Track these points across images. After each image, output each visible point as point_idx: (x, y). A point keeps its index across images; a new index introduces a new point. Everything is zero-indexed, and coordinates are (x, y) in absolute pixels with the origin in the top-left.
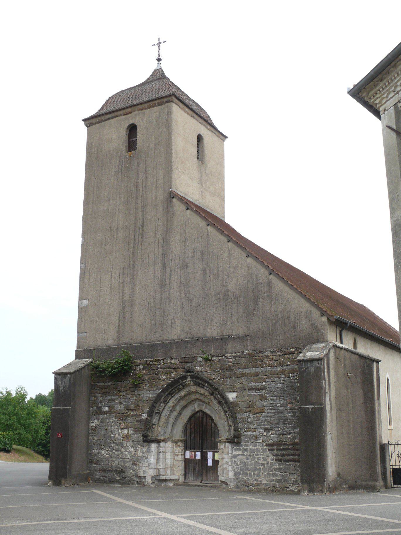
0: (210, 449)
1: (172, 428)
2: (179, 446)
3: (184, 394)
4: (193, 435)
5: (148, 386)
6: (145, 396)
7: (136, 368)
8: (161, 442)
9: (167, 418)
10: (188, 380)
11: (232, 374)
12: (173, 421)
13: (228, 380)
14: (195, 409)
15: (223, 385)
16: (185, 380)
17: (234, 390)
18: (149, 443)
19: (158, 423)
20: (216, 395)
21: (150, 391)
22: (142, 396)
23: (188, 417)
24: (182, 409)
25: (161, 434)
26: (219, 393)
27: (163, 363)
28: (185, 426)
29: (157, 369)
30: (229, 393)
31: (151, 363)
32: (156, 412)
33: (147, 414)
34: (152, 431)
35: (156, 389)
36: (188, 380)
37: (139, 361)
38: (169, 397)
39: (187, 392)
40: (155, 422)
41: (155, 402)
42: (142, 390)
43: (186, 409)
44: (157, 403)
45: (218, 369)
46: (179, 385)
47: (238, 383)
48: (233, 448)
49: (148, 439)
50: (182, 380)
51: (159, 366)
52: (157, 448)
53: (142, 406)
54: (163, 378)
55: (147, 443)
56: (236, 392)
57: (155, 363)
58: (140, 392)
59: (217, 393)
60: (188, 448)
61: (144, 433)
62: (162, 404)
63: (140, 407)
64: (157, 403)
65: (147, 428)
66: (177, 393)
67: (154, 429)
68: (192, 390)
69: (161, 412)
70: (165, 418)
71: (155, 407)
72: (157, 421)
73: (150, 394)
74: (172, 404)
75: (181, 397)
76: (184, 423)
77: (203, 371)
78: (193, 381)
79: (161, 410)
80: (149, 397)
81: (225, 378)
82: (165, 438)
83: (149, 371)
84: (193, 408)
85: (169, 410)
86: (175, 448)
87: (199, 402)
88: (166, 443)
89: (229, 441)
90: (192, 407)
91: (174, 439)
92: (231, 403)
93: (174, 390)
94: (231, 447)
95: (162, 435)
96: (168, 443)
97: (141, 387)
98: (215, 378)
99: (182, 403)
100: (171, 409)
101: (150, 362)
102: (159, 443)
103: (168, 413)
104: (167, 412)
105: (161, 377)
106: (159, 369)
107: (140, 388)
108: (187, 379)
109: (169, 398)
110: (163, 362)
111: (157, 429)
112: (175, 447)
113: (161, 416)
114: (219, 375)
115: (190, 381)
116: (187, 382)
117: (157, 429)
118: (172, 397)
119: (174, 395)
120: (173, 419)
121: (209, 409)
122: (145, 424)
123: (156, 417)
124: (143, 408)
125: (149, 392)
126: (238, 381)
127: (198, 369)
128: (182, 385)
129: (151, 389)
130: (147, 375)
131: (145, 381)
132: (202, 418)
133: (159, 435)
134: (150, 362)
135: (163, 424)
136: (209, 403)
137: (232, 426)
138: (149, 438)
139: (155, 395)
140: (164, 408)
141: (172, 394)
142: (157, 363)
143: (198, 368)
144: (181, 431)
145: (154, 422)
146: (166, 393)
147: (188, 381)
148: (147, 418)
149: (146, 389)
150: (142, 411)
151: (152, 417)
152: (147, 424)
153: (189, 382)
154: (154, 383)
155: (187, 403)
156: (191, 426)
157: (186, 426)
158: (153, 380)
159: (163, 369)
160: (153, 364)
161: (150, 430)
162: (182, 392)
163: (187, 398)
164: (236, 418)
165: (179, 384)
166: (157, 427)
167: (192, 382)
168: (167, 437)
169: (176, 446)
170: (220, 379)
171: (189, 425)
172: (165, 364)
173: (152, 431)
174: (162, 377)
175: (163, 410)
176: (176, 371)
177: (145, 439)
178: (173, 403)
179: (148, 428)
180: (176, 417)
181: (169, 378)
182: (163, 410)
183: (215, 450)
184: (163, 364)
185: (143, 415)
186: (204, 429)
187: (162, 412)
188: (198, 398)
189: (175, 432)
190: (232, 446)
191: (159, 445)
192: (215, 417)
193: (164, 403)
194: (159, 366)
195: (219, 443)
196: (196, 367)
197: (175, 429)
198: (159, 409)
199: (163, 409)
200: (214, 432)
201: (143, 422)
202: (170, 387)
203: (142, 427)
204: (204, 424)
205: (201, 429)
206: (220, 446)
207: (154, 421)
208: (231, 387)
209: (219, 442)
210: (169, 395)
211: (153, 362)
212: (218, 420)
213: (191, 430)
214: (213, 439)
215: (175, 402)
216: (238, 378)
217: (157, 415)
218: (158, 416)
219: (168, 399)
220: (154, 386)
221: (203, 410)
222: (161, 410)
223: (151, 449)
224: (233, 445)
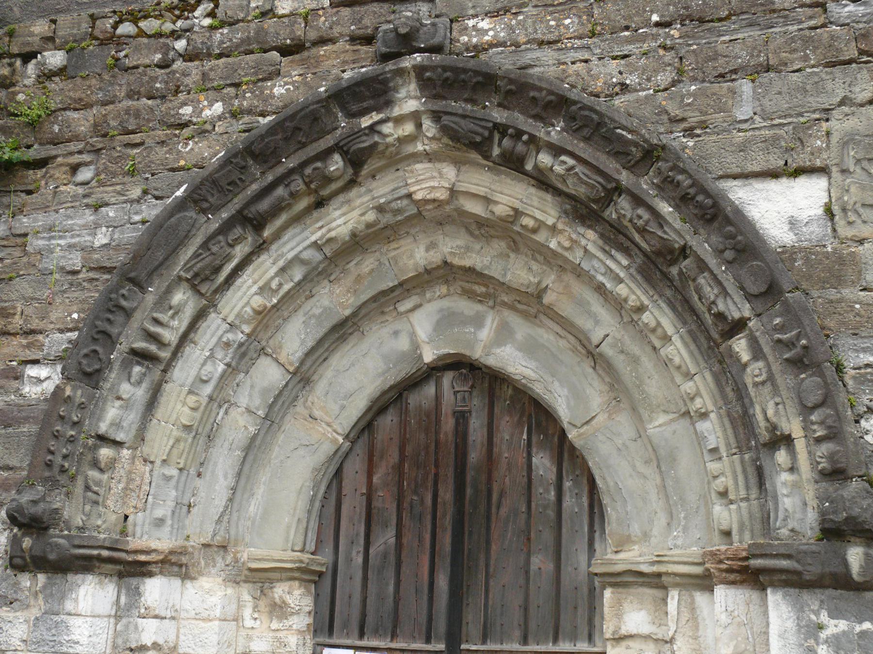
0: (517, 633)
1: (239, 474)
2: (279, 610)
3: (350, 226)
4: (385, 539)
5: (85, 174)
6: (62, 242)
7: (14, 72)
8: (151, 575)
9: (211, 399)
10: (396, 111)
11: (780, 41)
12: (252, 429)
13: (745, 87)
14: (416, 346)
15: (703, 125)
16: (378, 110)
17: (802, 159)
18: (58, 578)
19: (141, 437)
20: (638, 201)
21: (97, 208)
22: (41, 243)
23: (358, 406)
24: (320, 342)
25: (159, 513)
26: (666, 185)
27: (207, 22)
28: (332, 470)
29: (164, 65)
30: (758, 185)
31: (126, 28)
32: (134, 352)
33: (59, 368)
34: (87, 488)
35: (145, 192)
36: (396, 111)
37: (41, 27)
38: (238, 248)
39: (380, 209)
40: (117, 425)
41: (132, 275)
42: (45, 208)
43: (346, 347)
44: (140, 285)
45: (655, 18)
46: (325, 155)
47: (842, 103)
48: (821, 627)
49: (57, 545)
50: (354, 108)
51: (180, 45)
52: (118, 617)
53: (29, 311)
54: (207, 113)
55: (42, 578)
56: (823, 171)
57: (150, 25)
58: (25, 222)
59: (645, 185)
60: (345, 625)
61: (25, 498)
62: (179, 297)
63: (17, 322)
64: (143, 289)
65: (49, 465)
66: (297, 219)
67: (105, 477)
68: (419, 196)
69: (165, 354)
70: (192, 400)
71: (128, 314)
72: (132, 418)
73: (97, 226)
74: (258, 301)
75: (328, 251)
76: (327, 449)
77: (522, 39)
78: (436, 116)
79: (170, 336)
80: (87, 250)
81: (722, 76)
82: (180, 542)
83: (106, 77)
84: (403, 344)
85: (228, 344)
86: (249, 623)
87: (446, 303)
88: (189, 584)
89: (784, 563)
90: (396, 333)
91: (245, 557)
92: (789, 254)
93: (280, 191)
94: (791, 624)
95: (160, 522)
96: (205, 582)
97: (38, 189)
98: (631, 80)
99: (326, 302)
100: (240, 337)
101: (115, 26)
102: (134, 581)
103: (221, 367)
104: (211, 356)
105: (187, 110)
106: (179, 65)
107: (29, 192)
108: (389, 104)
109: (240, 251)
110: (211, 14)
111: (130, 480)
112: (247, 612)
113: (167, 387)
114: (669, 57)
115: (415, 117)
116: (387, 128)
117: (130, 480)
118: (260, 248)
119: (277, 236)
120: (249, 411)
121: (530, 348)
122: (39, 436)
123: (125, 389)
124: (35, 324)
125: (89, 217)
126: (840, 94)
127: (485, 32)
128: (345, 154)
129: (107, 193)
130: (88, 106)
131: (73, 147)
132: (461, 418)
133: (138, 519)
134: (115, 26)
135: (178, 440)
136: (539, 294)
137: (800, 445)
138: (58, 538)
139: (130, 235)
140: (193, 326)
141: (258, 224)
142: (168, 27)
143: (485, 24)
144: (302, 504)
145: (112, 424)
146: (215, 209)
147: (399, 121)
148: (58, 390)
149: (75, 197)
150: (28, 346)
151: (96, 387)
152: (56, 436)
153: (408, 128)
154: (136, 151)
155: (364, 297)
156: (370, 474)
157: (339, 473)
158: (133, 132)
159: (209, 55)
160: (142, 33)
161: (73, 478)
162: (337, 213)
163: (368, 264)
164: (839, 368)
165: (328, 141)
166: (133, 458)
167: (429, 127)
168: (195, 541)
169: (255, 608)
170: (674, 83)
171: (355, 468)
172: (223, 24)
173: (87, 488)
174: (198, 112)
175: (185, 338)
176: (303, 62)
177: (27, 542)
178: (264, 289)
179: (58, 460)
180: (277, 398)
181: (250, 112)
182: (185, 338)
183: (555, 641)
184: (212, 28)
185: (32, 371)
186: (469, 491)
187: (175, 354)
188: (456, 261)
189: (253, 508)
190: (800, 609)
191: (136, 593)
192: (577, 395)
193: (195, 288)
194: (180, 45)
195: (608, 593)
196: (471, 23)
197: (260, 491)
198: (158, 330)
199: (183, 329)
200: (551, 513)
201: (26, 419)
202: (255, 170)
203: (13, 462)
204: (474, 456)
205: (447, 494)
206: (619, 616)
207: (112, 412)
208: (776, 139)
209: (614, 585)
210: (238, 231)
211: (135, 21)
212: (601, 418)
213: (369, 497)
214: (540, 562)
215: (280, 285)
216: (833, 65)
217: (137, 369)
218: (139, 383)
219: (228, 258)
220: (132, 173)
221: (477, 354)
222: (170, 336)
223: (73, 621)
224: (812, 600)
